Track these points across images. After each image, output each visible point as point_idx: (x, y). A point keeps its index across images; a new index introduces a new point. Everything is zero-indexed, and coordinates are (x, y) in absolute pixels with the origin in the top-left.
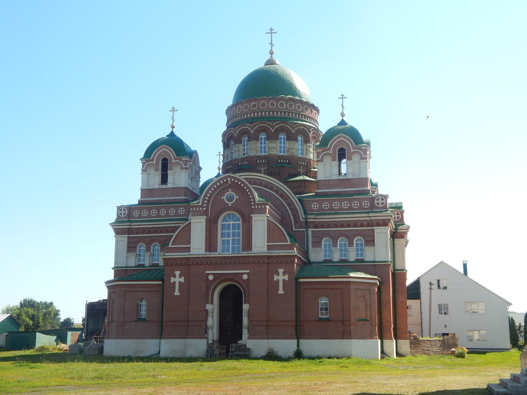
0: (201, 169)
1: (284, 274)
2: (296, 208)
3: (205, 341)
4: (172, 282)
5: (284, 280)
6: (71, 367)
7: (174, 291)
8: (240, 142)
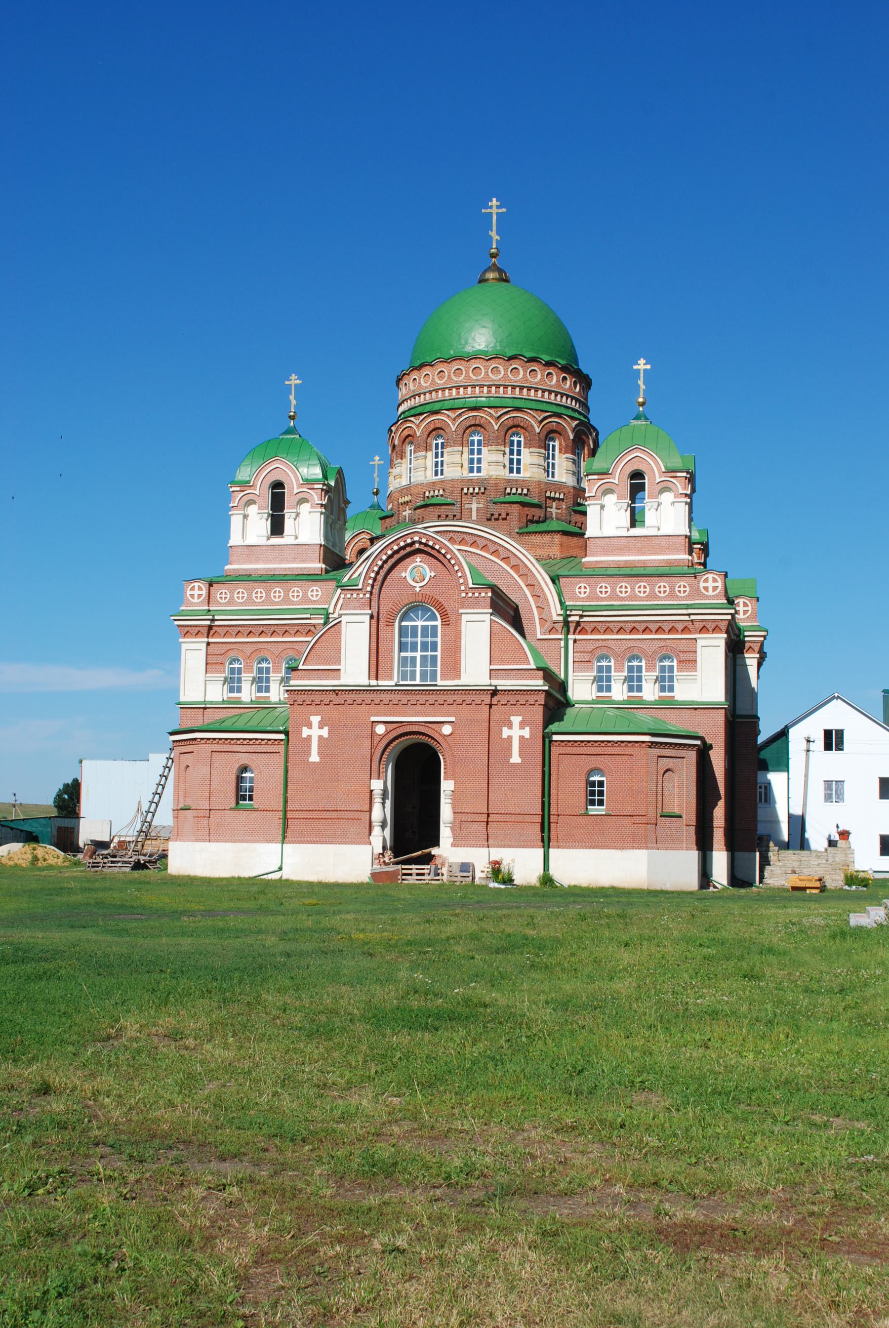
0: (349, 502)
1: (522, 726)
2: (544, 594)
3: (368, 848)
4: (304, 735)
5: (522, 738)
6: (783, 883)
7: (309, 754)
8: (427, 449)
